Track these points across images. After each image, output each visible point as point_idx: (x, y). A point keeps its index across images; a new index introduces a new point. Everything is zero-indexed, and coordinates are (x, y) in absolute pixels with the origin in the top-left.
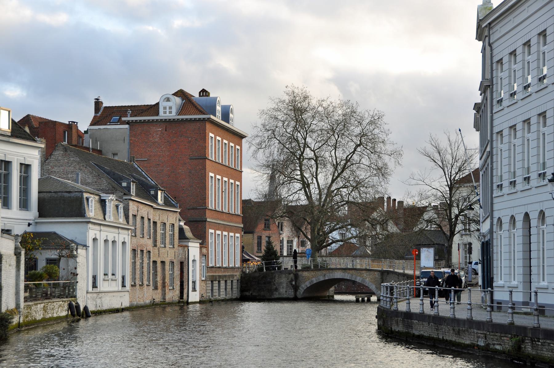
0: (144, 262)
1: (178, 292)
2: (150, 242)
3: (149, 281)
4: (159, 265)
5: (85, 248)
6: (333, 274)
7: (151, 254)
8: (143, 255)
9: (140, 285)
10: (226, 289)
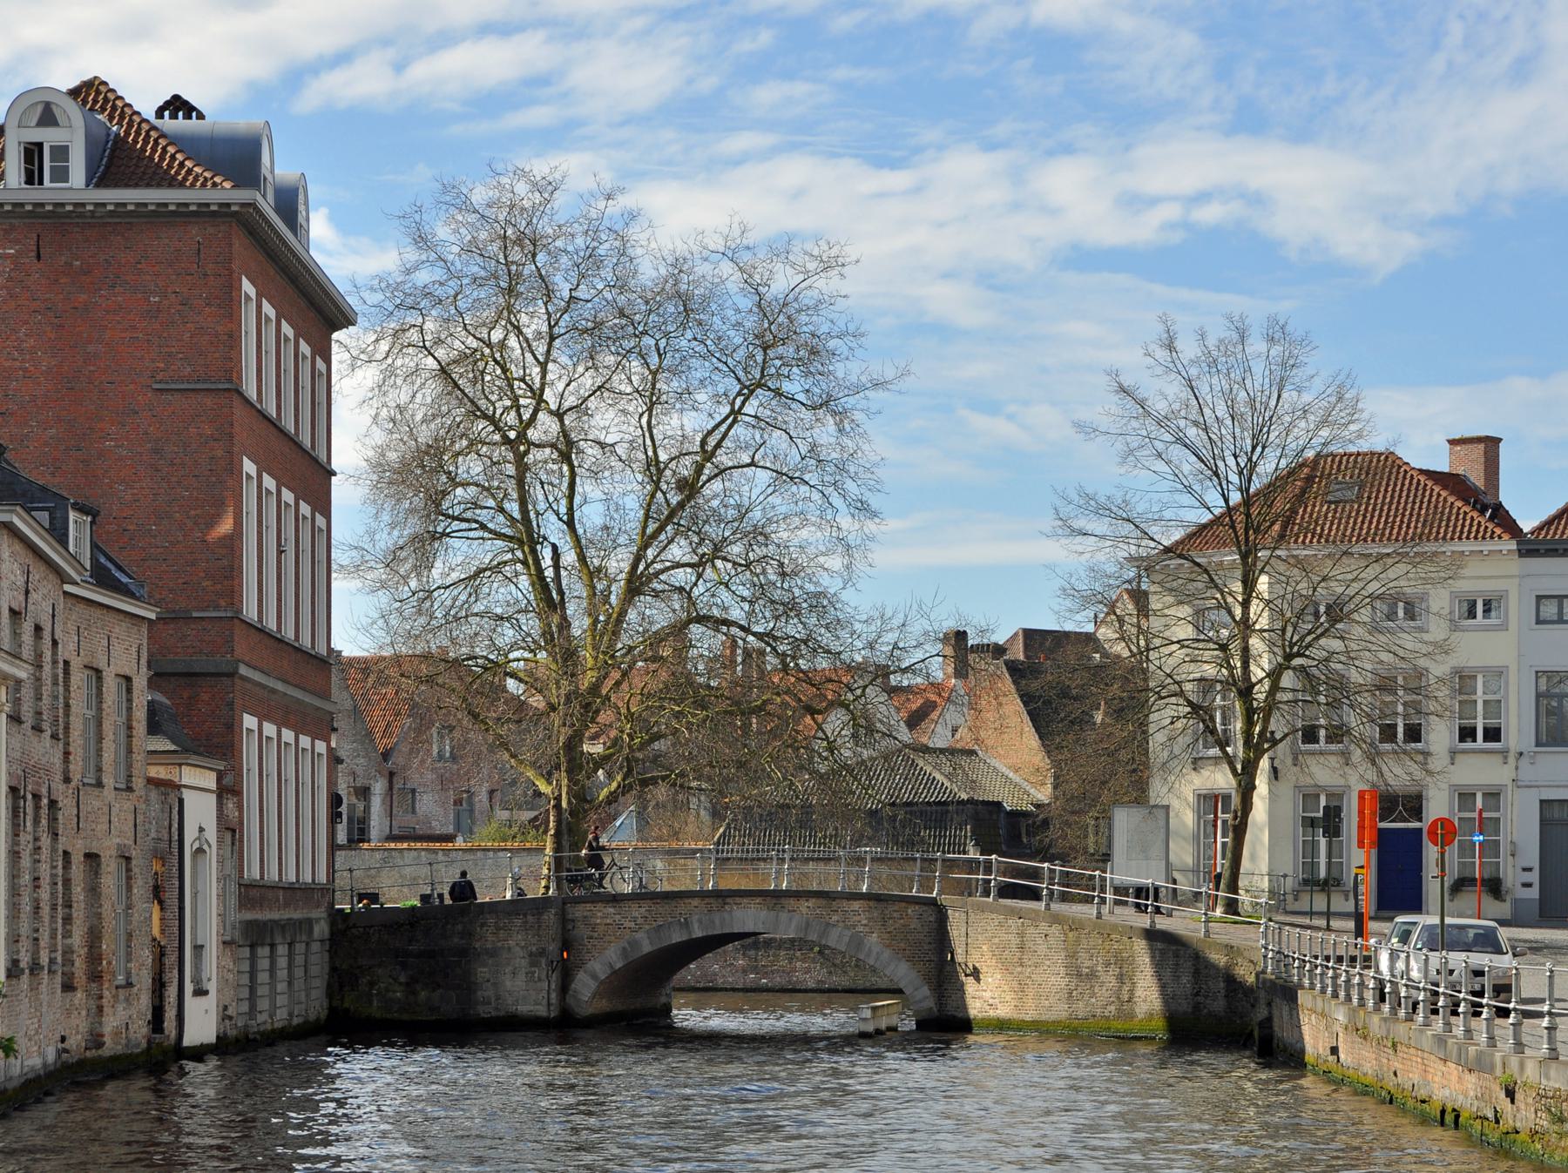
6: (726, 916)
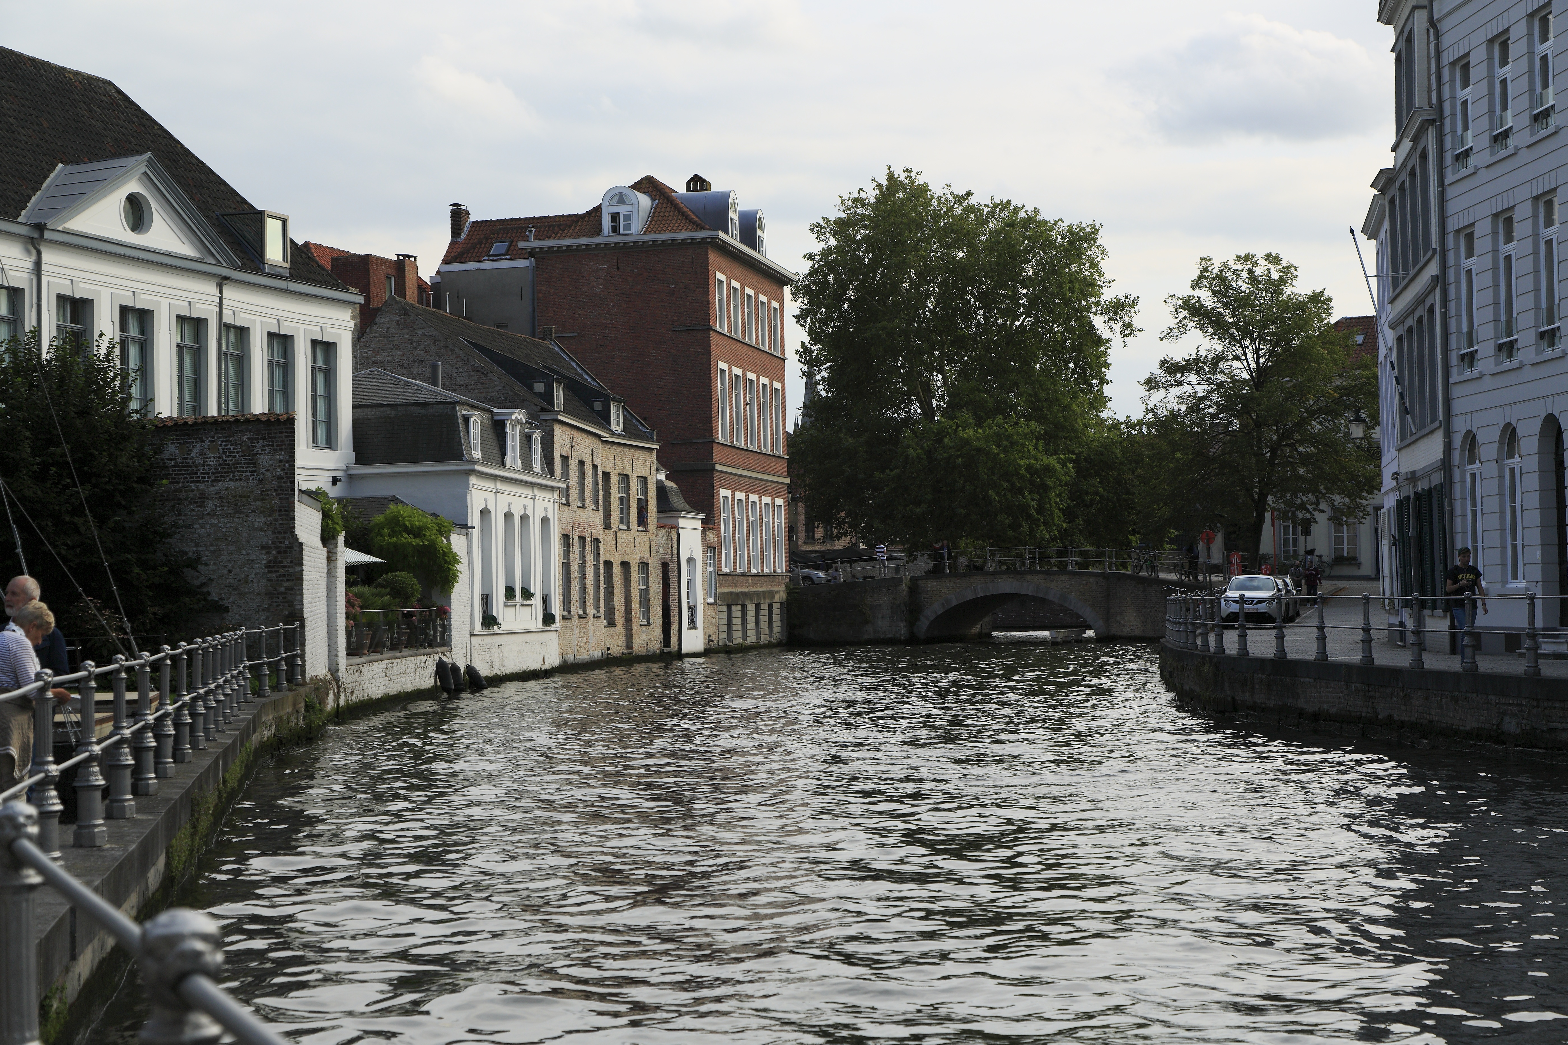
0: (587, 565)
1: (657, 632)
2: (598, 518)
3: (597, 608)
4: (617, 571)
5: (464, 531)
7: (601, 546)
8: (584, 548)
9: (580, 617)
10: (758, 622)
